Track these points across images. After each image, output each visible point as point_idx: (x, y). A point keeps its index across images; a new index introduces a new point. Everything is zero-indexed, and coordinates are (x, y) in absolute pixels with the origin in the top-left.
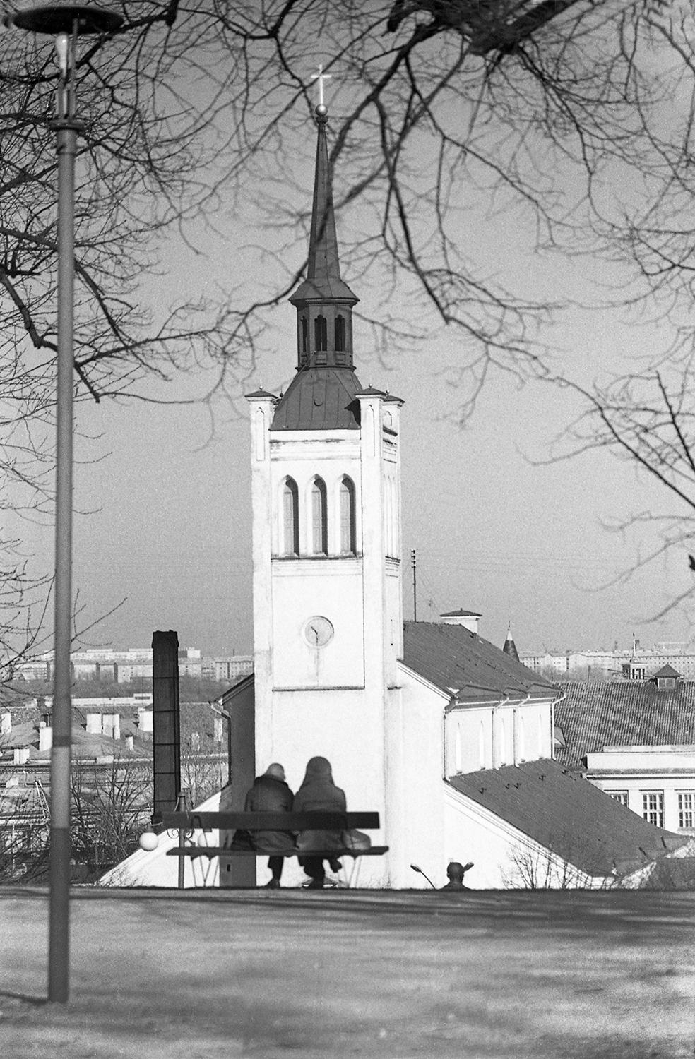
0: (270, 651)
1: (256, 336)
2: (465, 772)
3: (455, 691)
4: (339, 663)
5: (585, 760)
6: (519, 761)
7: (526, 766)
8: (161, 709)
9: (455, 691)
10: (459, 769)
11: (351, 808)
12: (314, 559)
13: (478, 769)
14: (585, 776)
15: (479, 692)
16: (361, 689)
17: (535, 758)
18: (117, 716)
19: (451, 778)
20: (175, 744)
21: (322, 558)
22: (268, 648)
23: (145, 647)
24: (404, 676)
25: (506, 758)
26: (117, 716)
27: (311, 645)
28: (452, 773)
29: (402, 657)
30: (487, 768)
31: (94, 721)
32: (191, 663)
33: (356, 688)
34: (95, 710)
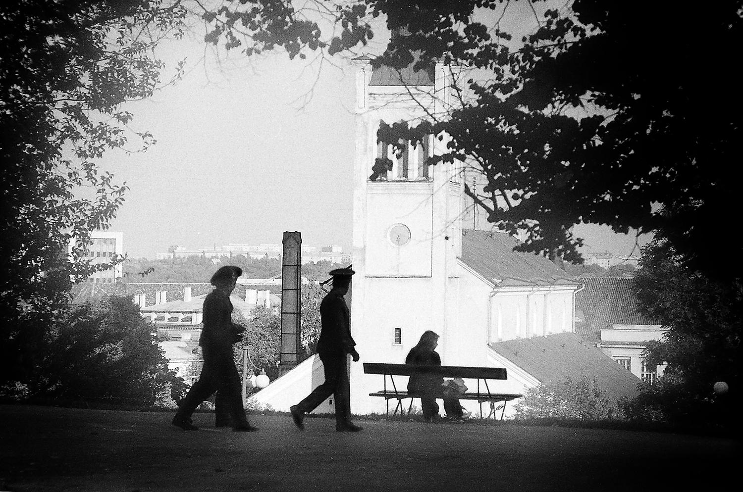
0: (364, 249)
1: (152, 41)
2: (504, 340)
3: (498, 281)
4: (413, 258)
5: (599, 335)
6: (547, 334)
7: (551, 338)
8: (288, 287)
9: (498, 281)
10: (500, 337)
11: (443, 364)
12: (397, 181)
13: (514, 338)
14: (599, 345)
15: (518, 283)
16: (429, 277)
17: (560, 331)
18: (268, 292)
19: (493, 344)
20: (297, 313)
21: (404, 181)
22: (363, 247)
23: (124, 248)
24: (459, 269)
25: (537, 330)
26: (268, 292)
27: (394, 245)
28: (494, 340)
29: (461, 256)
30: (522, 337)
31: (251, 294)
32: (309, 254)
33: (426, 277)
34: (251, 287)
